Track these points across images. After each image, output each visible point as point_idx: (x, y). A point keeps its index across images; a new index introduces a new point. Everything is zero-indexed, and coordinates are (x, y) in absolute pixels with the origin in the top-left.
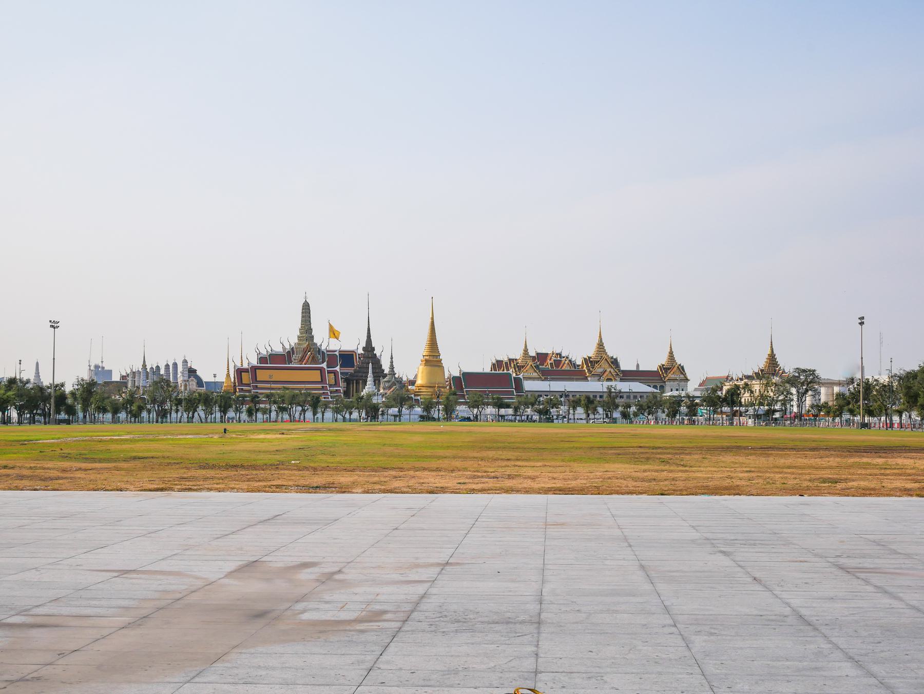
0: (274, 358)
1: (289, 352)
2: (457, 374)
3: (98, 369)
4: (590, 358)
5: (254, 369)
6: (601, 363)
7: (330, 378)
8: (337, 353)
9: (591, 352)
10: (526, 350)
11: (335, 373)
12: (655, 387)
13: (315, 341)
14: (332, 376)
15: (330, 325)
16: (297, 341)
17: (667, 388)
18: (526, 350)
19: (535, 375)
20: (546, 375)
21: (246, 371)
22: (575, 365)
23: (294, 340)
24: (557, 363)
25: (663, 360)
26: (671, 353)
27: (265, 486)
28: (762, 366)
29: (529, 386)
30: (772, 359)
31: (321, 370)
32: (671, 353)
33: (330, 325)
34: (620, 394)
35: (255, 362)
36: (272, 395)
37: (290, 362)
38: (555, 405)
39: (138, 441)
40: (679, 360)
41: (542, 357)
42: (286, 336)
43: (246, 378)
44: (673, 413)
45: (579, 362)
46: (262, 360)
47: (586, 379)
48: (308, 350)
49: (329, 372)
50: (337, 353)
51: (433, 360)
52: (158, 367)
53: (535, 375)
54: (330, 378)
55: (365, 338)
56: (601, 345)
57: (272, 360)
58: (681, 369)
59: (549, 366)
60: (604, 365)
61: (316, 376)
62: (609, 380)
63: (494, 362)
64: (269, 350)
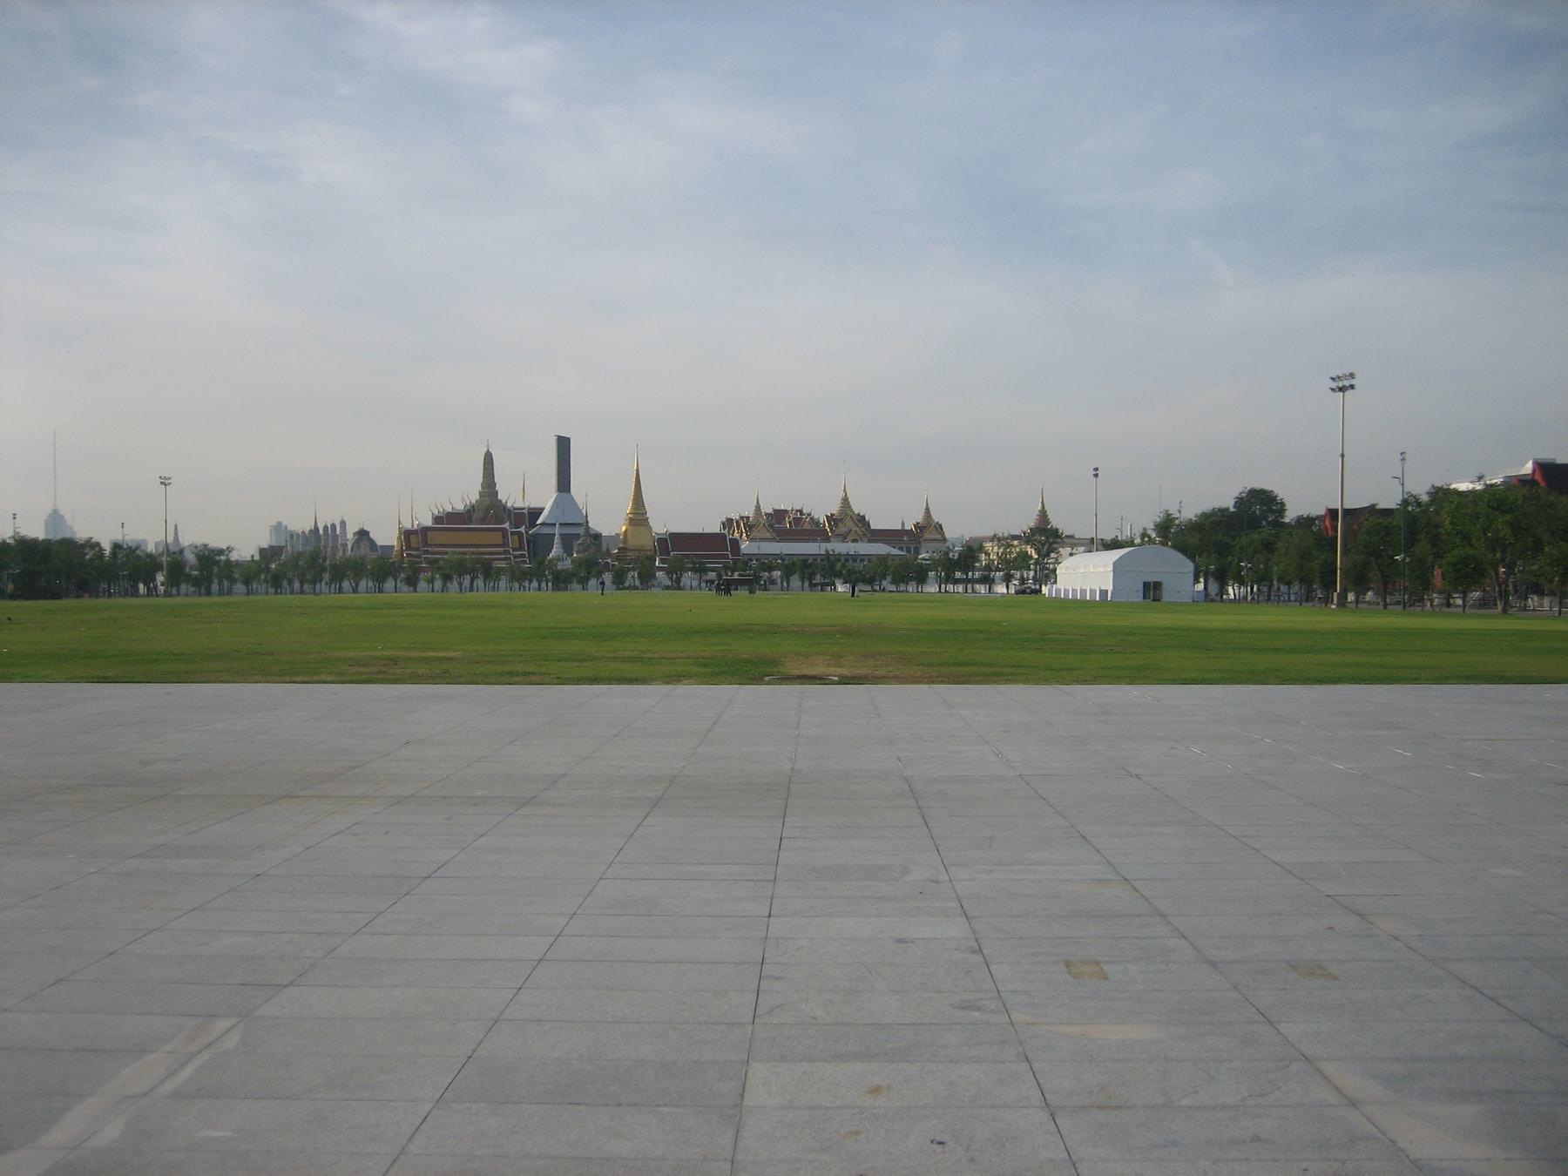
0: (452, 517)
3: (278, 528)
5: (425, 530)
6: (847, 522)
7: (513, 541)
9: (834, 509)
10: (758, 506)
11: (520, 534)
12: (901, 549)
14: (413, 545)
17: (923, 550)
18: (758, 506)
19: (768, 535)
20: (783, 536)
21: (415, 532)
22: (818, 523)
23: (474, 497)
24: (797, 521)
25: (919, 518)
26: (927, 509)
27: (502, 674)
28: (1032, 524)
29: (745, 546)
30: (1043, 515)
31: (504, 531)
32: (927, 509)
34: (838, 557)
35: (429, 522)
36: (436, 561)
37: (471, 522)
38: (770, 569)
40: (936, 517)
41: (779, 515)
42: (463, 493)
44: (619, 581)
45: (822, 519)
46: (437, 519)
47: (828, 540)
48: (490, 508)
51: (638, 517)
52: (334, 526)
53: (768, 535)
56: (845, 500)
57: (448, 520)
58: (939, 528)
59: (782, 524)
60: (850, 524)
62: (855, 541)
64: (170, 539)
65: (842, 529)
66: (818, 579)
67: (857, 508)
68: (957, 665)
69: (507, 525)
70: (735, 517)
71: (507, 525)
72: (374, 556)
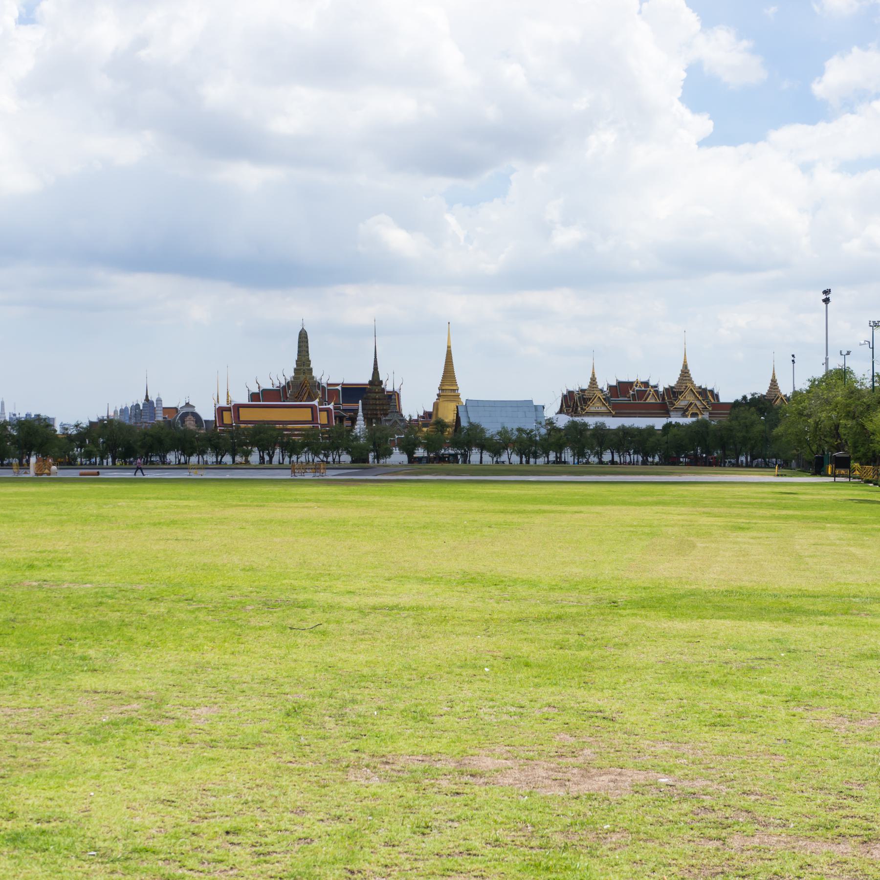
0: (266, 394)
1: (284, 387)
2: (257, 391)
4: (672, 388)
5: (238, 407)
7: (323, 418)
8: (339, 388)
11: (328, 411)
13: (314, 374)
15: (685, 366)
16: (293, 374)
20: (619, 411)
21: (228, 409)
23: (290, 374)
31: (313, 407)
33: (685, 366)
35: (245, 400)
37: (286, 399)
39: (538, 620)
41: (622, 388)
43: (227, 418)
46: (254, 397)
49: (321, 410)
50: (339, 388)
53: (603, 409)
54: (323, 418)
55: (372, 370)
57: (262, 397)
59: (626, 396)
60: (690, 398)
61: (306, 415)
63: (565, 393)
65: (681, 403)
66: (420, 452)
67: (699, 380)
68: (545, 512)
69: (316, 403)
70: (652, 383)
71: (316, 403)
72: (563, 433)
